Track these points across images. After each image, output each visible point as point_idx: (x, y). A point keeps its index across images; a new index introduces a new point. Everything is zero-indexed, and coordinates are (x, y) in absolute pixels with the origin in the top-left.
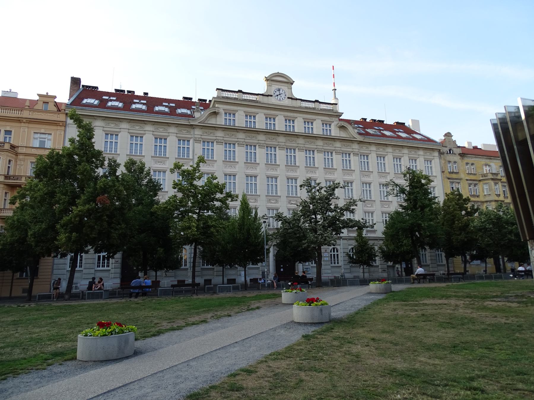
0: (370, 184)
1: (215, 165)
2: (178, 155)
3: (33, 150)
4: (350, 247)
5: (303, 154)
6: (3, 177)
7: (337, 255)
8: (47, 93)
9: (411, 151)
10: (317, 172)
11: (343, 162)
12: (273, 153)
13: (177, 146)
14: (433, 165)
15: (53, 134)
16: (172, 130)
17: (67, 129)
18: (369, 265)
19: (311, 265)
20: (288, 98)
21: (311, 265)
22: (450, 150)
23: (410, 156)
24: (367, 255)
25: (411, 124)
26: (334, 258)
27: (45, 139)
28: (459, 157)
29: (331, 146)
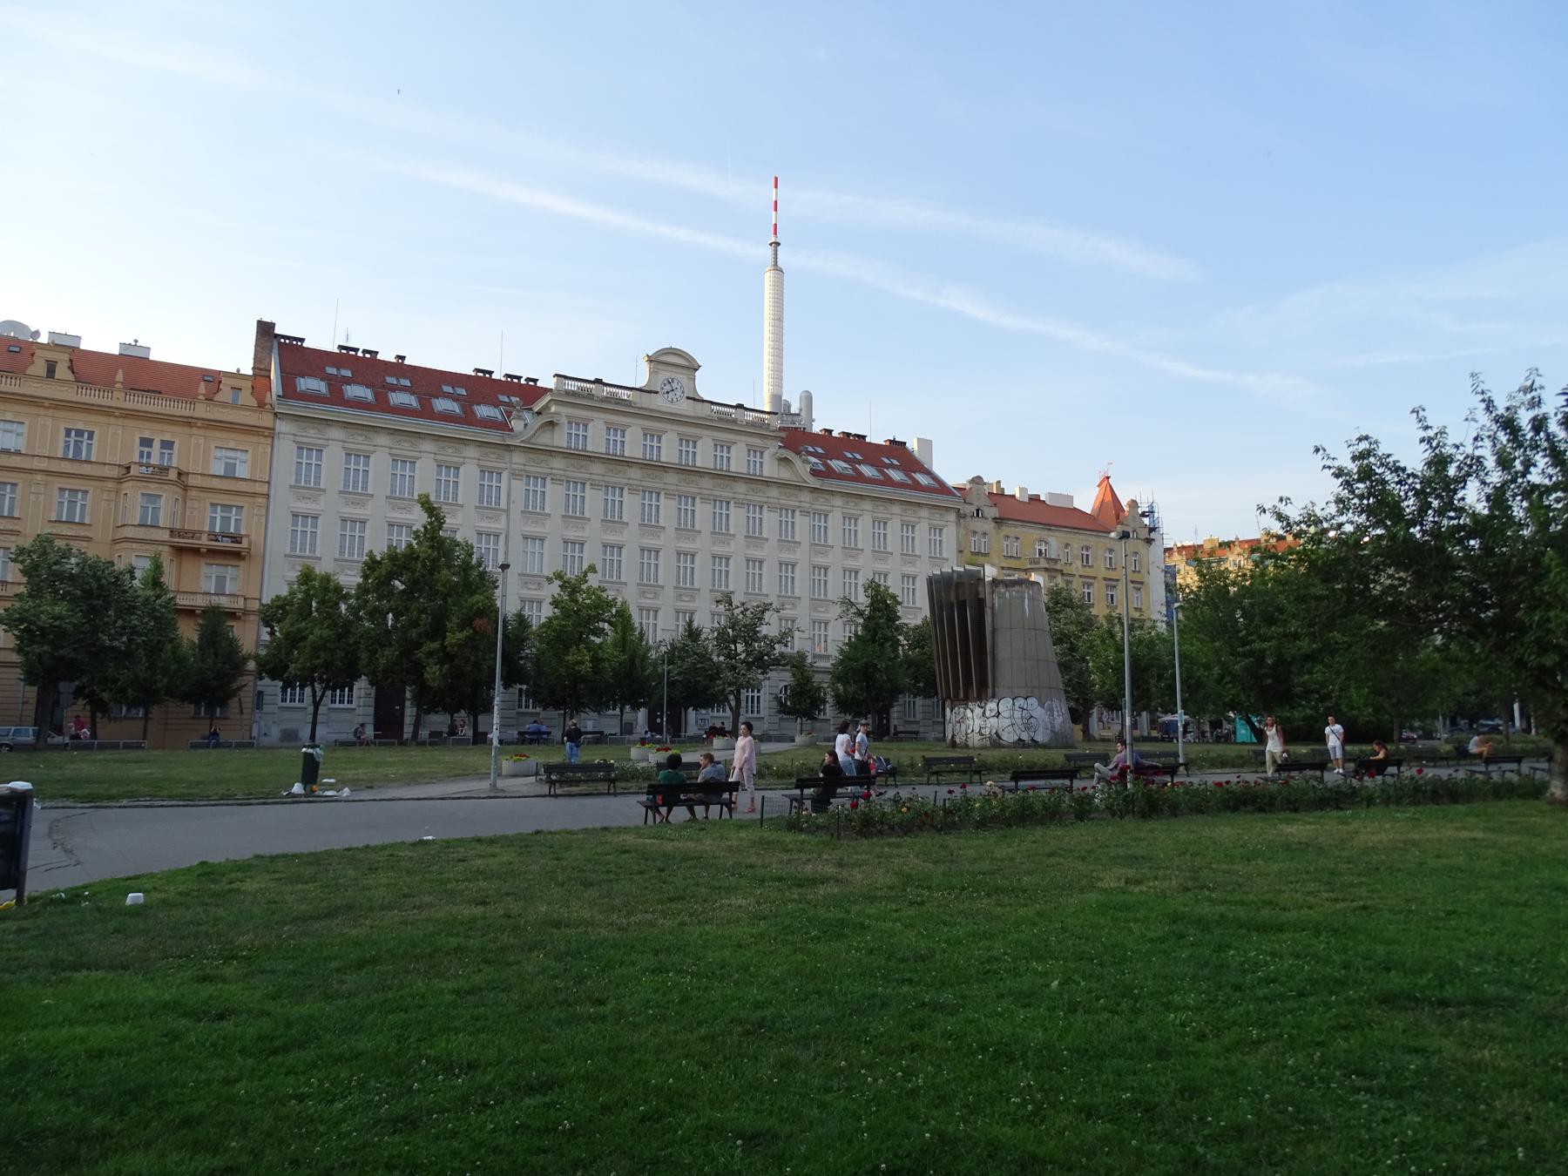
0: (826, 569)
1: (587, 527)
2: (345, 485)
3: (214, 480)
4: (782, 684)
5: (709, 508)
6: (168, 532)
7: (759, 697)
8: (238, 370)
9: (847, 502)
10: (733, 542)
11: (715, 518)
12: (579, 494)
13: (295, 460)
14: (917, 534)
15: (27, 423)
16: (472, 452)
17: (276, 441)
18: (811, 717)
19: (711, 714)
20: (688, 398)
21: (711, 714)
22: (978, 511)
23: (932, 522)
24: (808, 701)
25: (916, 448)
26: (752, 702)
27: (236, 459)
28: (994, 524)
29: (620, 475)
